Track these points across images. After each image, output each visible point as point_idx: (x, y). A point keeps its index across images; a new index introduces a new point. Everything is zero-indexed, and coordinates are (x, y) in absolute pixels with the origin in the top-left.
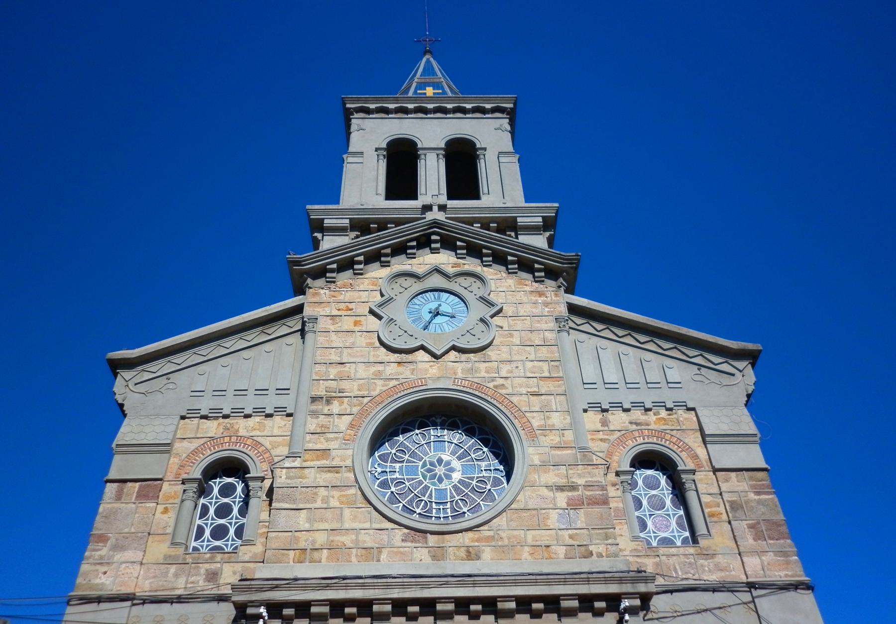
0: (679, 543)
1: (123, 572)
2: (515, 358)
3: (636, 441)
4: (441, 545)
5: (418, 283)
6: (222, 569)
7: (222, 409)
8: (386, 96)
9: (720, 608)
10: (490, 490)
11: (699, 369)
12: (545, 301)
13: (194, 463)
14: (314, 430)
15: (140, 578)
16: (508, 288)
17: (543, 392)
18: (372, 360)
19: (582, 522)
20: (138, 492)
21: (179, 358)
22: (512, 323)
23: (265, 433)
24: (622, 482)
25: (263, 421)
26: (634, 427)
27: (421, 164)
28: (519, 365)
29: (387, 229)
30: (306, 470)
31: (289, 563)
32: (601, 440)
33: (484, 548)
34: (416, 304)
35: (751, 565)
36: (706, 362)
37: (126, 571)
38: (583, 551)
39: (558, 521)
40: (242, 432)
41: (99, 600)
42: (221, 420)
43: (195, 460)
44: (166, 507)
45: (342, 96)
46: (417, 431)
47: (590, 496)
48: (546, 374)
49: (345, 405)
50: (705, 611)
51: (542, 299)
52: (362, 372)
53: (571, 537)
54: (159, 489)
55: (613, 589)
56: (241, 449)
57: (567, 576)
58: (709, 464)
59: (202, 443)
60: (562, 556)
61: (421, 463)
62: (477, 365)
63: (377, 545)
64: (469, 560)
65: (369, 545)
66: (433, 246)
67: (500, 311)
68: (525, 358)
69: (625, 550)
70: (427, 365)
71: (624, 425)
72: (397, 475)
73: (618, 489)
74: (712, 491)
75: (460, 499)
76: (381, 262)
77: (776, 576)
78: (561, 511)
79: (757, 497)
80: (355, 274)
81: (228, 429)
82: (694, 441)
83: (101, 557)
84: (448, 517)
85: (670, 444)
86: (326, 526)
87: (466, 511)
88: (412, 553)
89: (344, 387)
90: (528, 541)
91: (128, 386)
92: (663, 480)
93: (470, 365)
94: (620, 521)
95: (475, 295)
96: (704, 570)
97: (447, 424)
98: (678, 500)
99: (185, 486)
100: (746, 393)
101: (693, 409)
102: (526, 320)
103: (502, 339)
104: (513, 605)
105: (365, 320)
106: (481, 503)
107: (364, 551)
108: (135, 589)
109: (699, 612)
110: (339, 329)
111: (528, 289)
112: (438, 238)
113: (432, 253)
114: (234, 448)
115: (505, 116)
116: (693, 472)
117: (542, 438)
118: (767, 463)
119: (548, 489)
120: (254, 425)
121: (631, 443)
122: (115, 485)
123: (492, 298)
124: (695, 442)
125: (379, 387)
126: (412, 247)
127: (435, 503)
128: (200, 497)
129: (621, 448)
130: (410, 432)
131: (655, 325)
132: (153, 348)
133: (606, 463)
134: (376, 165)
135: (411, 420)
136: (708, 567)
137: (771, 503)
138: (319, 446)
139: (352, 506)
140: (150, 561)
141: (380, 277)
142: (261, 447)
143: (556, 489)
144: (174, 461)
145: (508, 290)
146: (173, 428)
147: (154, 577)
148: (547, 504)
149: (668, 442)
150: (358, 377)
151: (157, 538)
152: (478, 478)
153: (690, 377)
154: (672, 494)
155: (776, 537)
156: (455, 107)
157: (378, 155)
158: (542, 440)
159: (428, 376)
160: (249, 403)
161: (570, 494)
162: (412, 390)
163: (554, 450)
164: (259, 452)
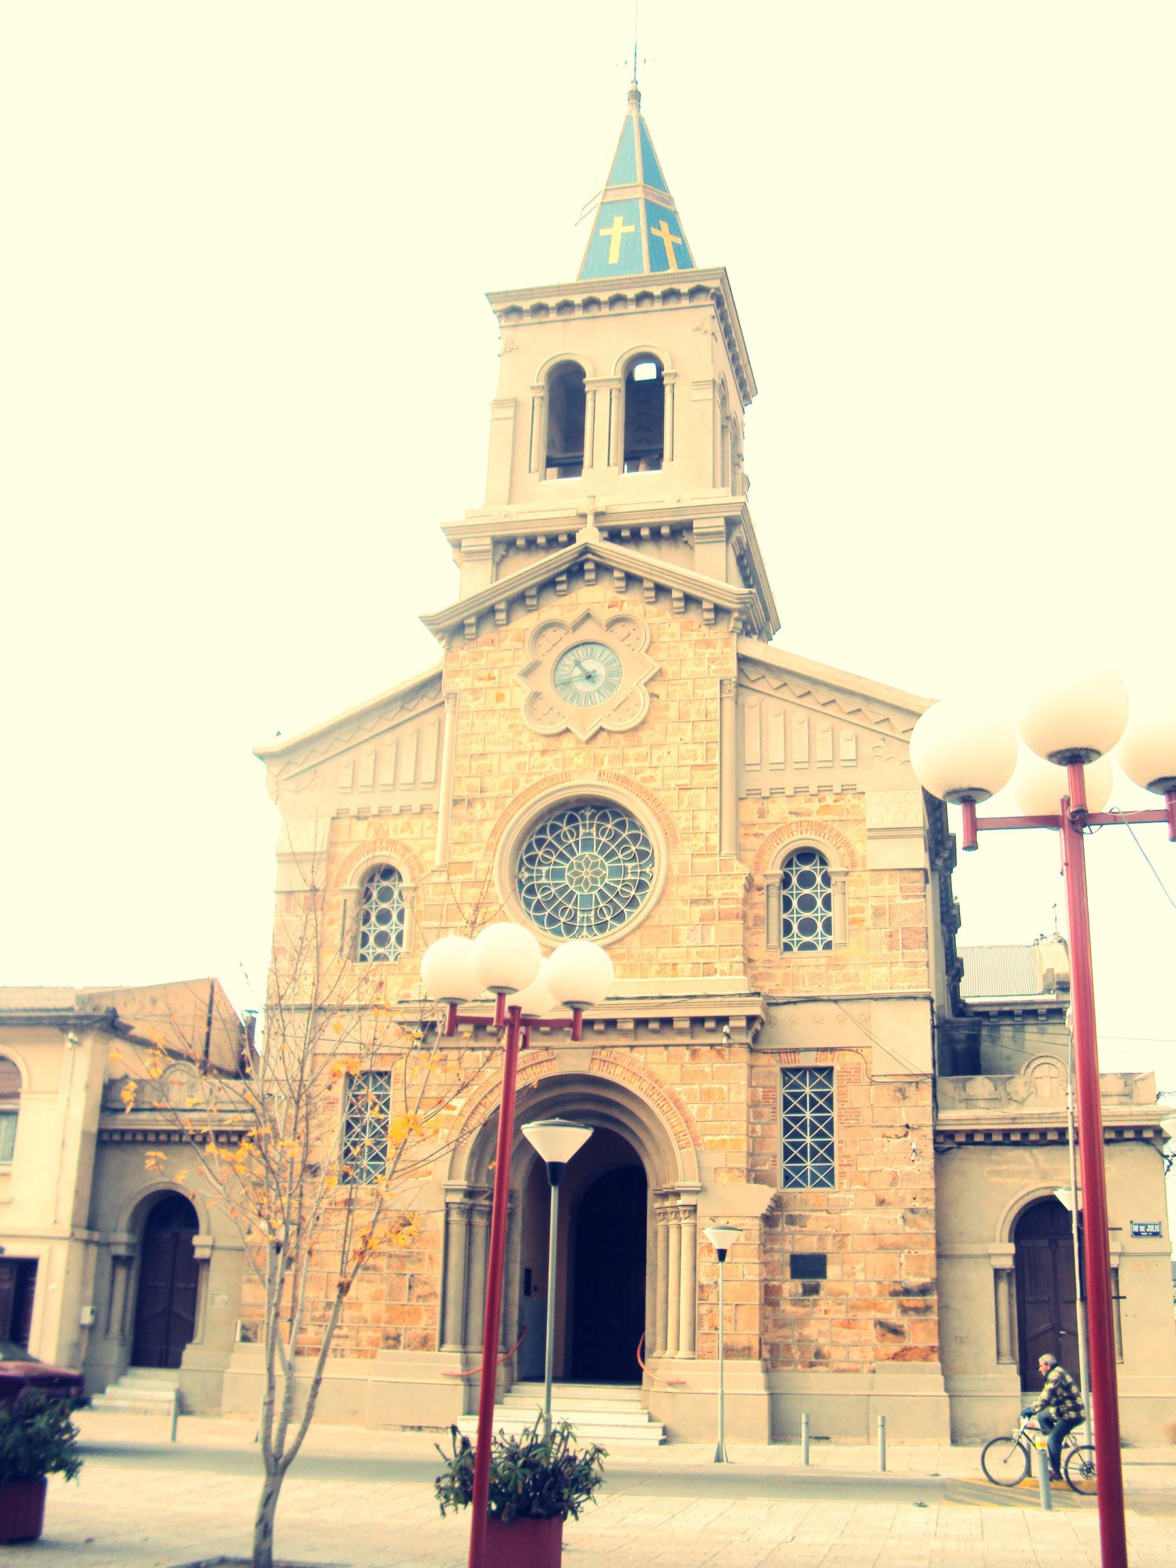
26: (794, 818)
48: (699, 761)
72: (543, 880)
106: (625, 910)
138: (463, 859)
161: (704, 908)
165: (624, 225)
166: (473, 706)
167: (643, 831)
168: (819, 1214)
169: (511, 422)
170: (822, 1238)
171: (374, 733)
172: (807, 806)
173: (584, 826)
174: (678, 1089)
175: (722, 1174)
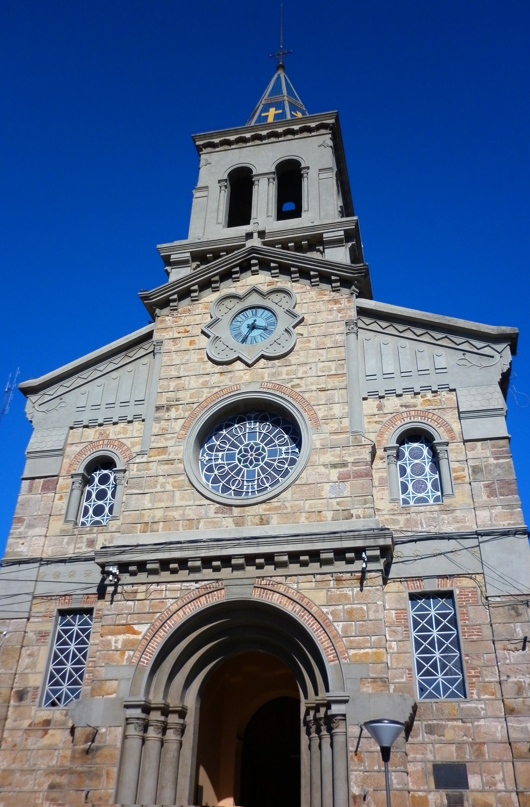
0: (431, 501)
1: (34, 543)
2: (310, 360)
3: (404, 421)
4: (243, 515)
5: (240, 303)
6: (97, 538)
7: (97, 420)
8: (227, 129)
9: (452, 552)
10: (287, 468)
11: (464, 354)
12: (340, 307)
13: (79, 462)
14: (157, 432)
15: (45, 546)
16: (310, 300)
17: (329, 387)
18: (201, 372)
19: (348, 491)
20: (42, 486)
21: (68, 383)
22: (311, 330)
23: (128, 435)
24: (388, 456)
25: (126, 426)
26: (404, 409)
27: (255, 189)
28: (313, 366)
29: (220, 257)
30: (151, 464)
31: (137, 533)
32: (376, 422)
33: (272, 515)
34: (238, 321)
35: (482, 517)
36: (471, 348)
37: (36, 542)
38: (346, 514)
39: (330, 492)
40: (112, 436)
41: (20, 562)
42: (97, 428)
43: (80, 459)
44: (62, 495)
45: (193, 135)
46: (236, 426)
47: (357, 470)
48: (333, 372)
49: (180, 411)
50: (441, 554)
51: (337, 306)
52: (194, 383)
53: (338, 504)
54: (56, 483)
55: (359, 543)
56: (110, 449)
57: (325, 536)
58: (461, 436)
59: (85, 446)
60: (330, 519)
61: (238, 451)
62: (280, 369)
63: (197, 517)
64: (261, 525)
65: (191, 517)
66: (253, 269)
67: (302, 320)
68: (318, 360)
69: (384, 510)
70: (242, 373)
72: (220, 461)
73: (384, 462)
74: (460, 459)
75: (264, 477)
76: (213, 288)
77: (500, 525)
78: (332, 484)
79: (496, 462)
80: (192, 301)
81: (102, 434)
82: (451, 417)
83: (20, 533)
84: (255, 491)
85: (431, 421)
86: (163, 505)
87: (268, 486)
88: (221, 522)
89: (180, 397)
90: (306, 508)
91: (34, 407)
92: (425, 450)
93: (274, 370)
94: (383, 487)
95: (284, 309)
96: (444, 523)
97: (259, 418)
98: (436, 467)
99: (73, 479)
100: (501, 372)
101: (454, 390)
103: (301, 345)
104: (286, 558)
105: (198, 339)
106: (280, 479)
107: (188, 522)
108: (42, 554)
109: (435, 556)
110: (178, 349)
111: (326, 298)
112: (256, 261)
113: (253, 275)
114: (106, 449)
115: (328, 131)
116: (447, 444)
117: (325, 426)
118: (509, 433)
119: (325, 467)
120: (120, 430)
121: (399, 423)
122: (28, 482)
123: (297, 310)
124: (452, 418)
125: (206, 393)
126: (236, 272)
127: (246, 481)
128: (85, 486)
129: (391, 427)
130: (229, 427)
131: (429, 320)
132: (49, 377)
133: (372, 443)
134: (218, 196)
135: (232, 416)
136: (447, 521)
137: (506, 466)
138: (160, 445)
139: (181, 489)
140: (51, 534)
141: (211, 301)
142: (124, 446)
143: (331, 467)
144: (66, 461)
145: (310, 301)
146: (64, 437)
147: (55, 545)
148: (323, 479)
149: (430, 420)
150: (190, 387)
151: (56, 518)
152: (279, 459)
153: (455, 362)
154: (431, 461)
156: (285, 130)
157: (220, 187)
158: (324, 427)
159: (242, 382)
160: (116, 414)
161: (341, 470)
162: (229, 395)
163: (333, 435)
167: (293, 425)
168: (455, 723)
170: (460, 745)
171: (104, 372)
172: (413, 401)
174: (325, 610)
175: (367, 685)
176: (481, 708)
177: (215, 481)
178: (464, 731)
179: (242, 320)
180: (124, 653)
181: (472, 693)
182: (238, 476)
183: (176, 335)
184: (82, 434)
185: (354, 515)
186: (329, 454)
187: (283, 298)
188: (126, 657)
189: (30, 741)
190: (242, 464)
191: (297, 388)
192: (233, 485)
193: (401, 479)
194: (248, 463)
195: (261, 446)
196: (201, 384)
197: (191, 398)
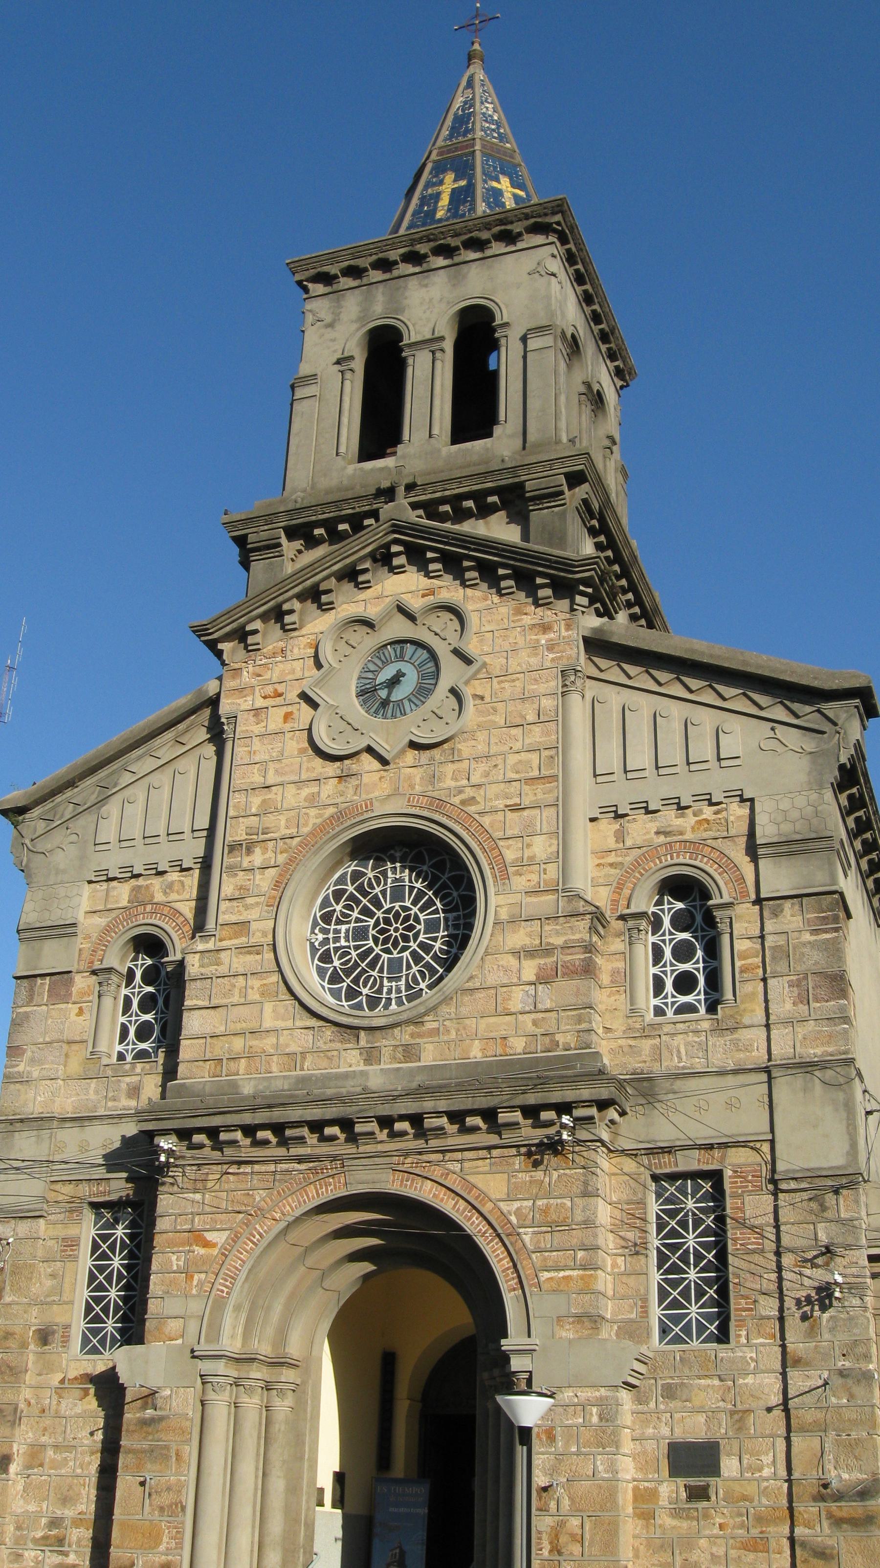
2: (494, 749)
11: (773, 729)
18: (304, 777)
26: (662, 839)
40: (159, 897)
51: (547, 637)
52: (292, 797)
71: (648, 837)
72: (343, 943)
89: (268, 825)
102: (518, 679)
107: (286, 1058)
111: (527, 620)
125: (314, 818)
127: (388, 978)
155: (826, 998)
157: (342, 372)
161: (542, 961)
164: (177, 924)
165: (455, 181)
166: (257, 729)
169: (766, 1085)
172: (679, 821)
173: (457, 918)
176: (751, 1358)
177: (335, 978)
178: (721, 1392)
179: (377, 669)
180: (192, 1277)
181: (739, 1336)
182: (374, 970)
183: (260, 703)
184: (107, 895)
185: (561, 1043)
186: (522, 932)
187: (449, 623)
188: (195, 1282)
189: (64, 1403)
190: (380, 947)
191: (471, 805)
192: (365, 986)
193: (653, 970)
194: (389, 945)
195: (412, 912)
196: (305, 800)
197: (287, 827)
